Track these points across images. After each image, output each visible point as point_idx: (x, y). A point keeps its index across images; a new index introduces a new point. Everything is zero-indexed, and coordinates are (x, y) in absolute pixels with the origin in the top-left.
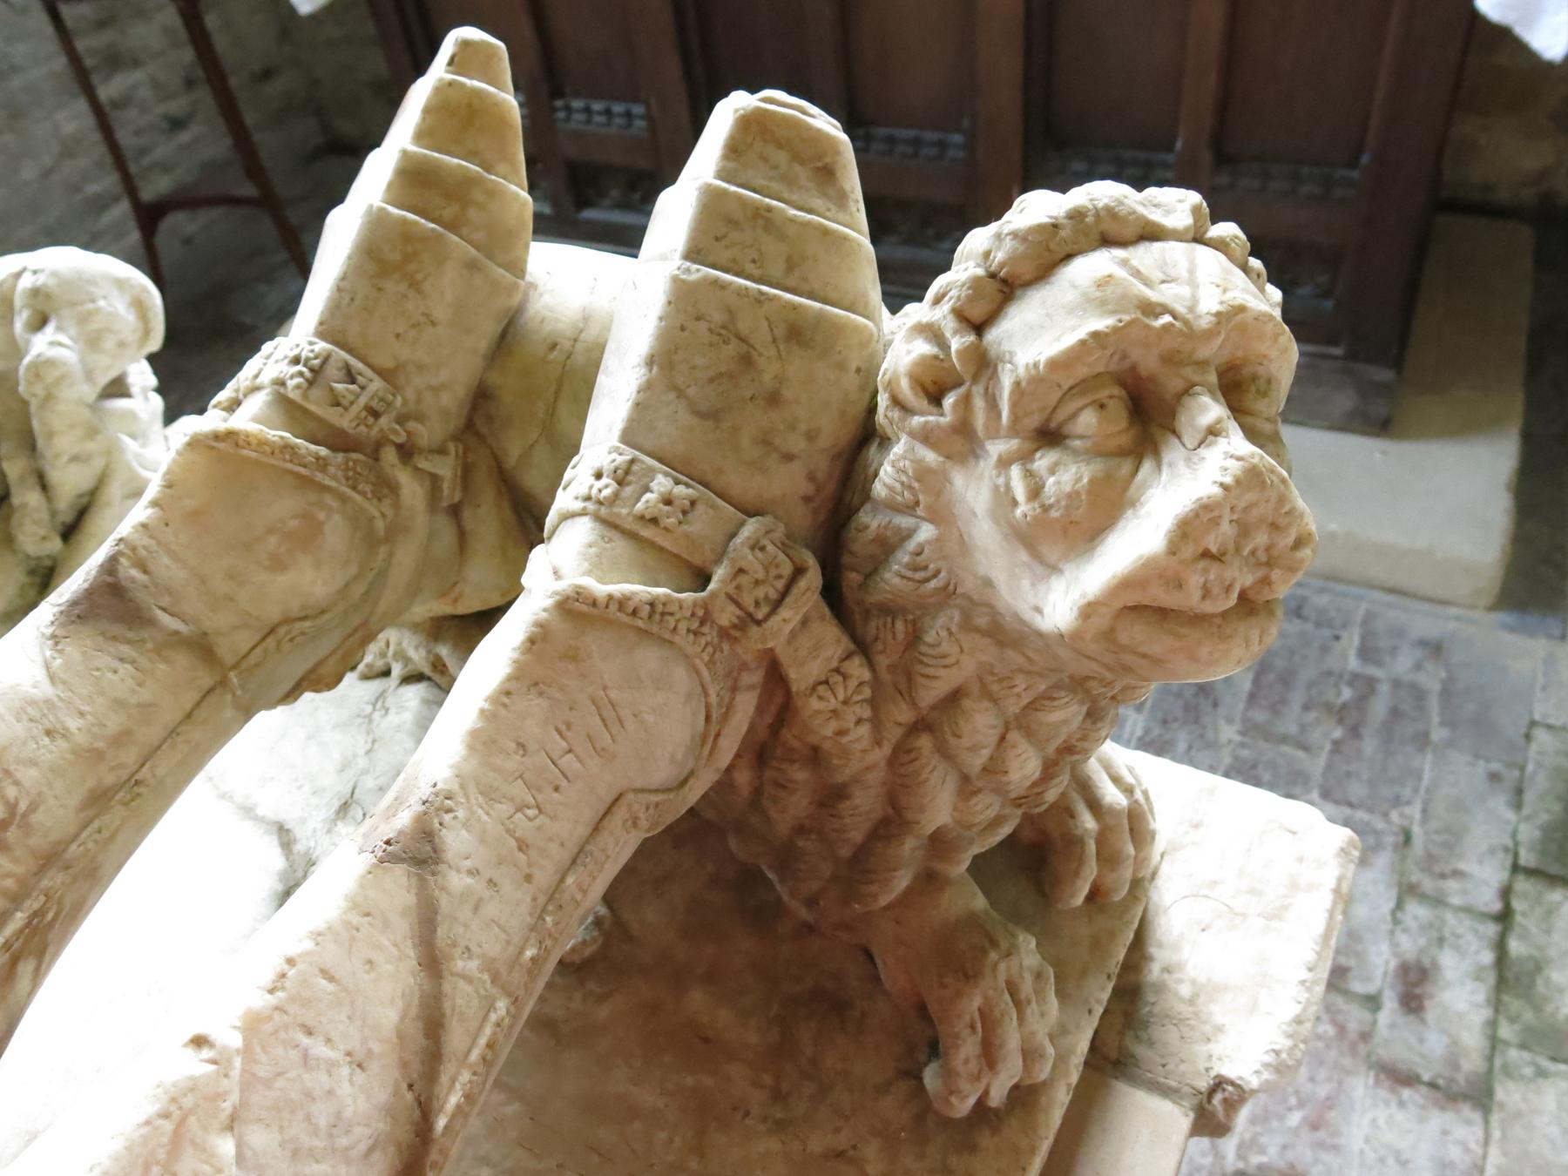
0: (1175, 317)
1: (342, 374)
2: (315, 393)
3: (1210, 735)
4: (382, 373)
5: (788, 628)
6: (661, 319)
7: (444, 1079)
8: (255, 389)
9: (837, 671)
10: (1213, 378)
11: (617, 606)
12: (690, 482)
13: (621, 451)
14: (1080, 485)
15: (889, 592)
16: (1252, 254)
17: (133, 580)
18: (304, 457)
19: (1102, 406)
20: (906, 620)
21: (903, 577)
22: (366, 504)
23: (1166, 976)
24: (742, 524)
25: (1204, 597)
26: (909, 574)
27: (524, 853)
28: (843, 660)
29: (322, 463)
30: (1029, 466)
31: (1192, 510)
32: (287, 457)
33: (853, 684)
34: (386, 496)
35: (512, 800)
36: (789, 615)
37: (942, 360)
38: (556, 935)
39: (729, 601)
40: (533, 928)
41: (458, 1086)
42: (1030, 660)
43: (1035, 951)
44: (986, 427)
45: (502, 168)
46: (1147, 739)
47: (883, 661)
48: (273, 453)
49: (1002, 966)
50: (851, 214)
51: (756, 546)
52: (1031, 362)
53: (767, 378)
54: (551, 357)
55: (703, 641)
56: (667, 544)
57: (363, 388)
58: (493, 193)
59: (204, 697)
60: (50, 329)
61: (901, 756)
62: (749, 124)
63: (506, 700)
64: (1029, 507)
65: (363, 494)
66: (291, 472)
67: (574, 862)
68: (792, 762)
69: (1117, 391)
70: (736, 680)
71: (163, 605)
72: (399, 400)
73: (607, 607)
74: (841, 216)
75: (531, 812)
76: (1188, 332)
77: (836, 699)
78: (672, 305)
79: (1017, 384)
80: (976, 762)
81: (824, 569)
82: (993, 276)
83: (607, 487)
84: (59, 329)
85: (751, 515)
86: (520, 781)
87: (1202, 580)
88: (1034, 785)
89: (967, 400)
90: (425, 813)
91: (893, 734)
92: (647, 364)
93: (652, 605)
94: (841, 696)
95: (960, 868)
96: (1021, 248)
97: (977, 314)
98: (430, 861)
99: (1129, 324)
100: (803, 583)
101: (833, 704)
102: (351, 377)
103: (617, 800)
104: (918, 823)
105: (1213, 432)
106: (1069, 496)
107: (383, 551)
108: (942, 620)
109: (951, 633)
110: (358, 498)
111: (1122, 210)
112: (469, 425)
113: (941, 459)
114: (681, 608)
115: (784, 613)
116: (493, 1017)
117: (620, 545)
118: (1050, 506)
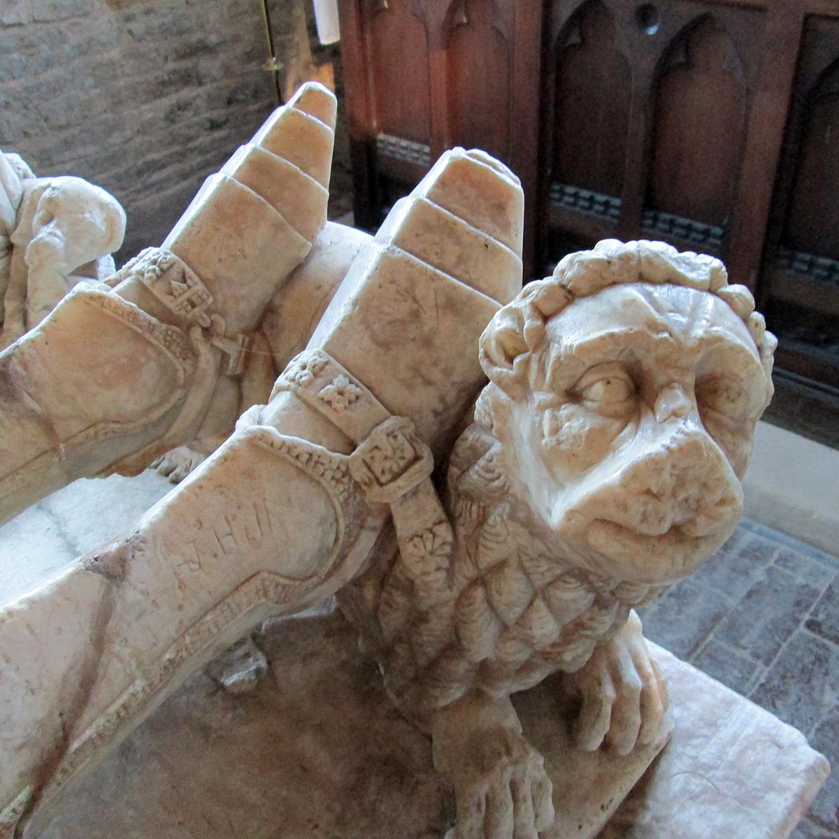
0: (671, 335)
1: (180, 277)
2: (160, 284)
3: (816, 695)
4: (203, 280)
5: (401, 493)
6: (369, 278)
7: (86, 717)
8: (129, 275)
9: (430, 530)
10: (690, 379)
11: (287, 449)
12: (360, 384)
13: (322, 355)
14: (582, 431)
15: (471, 484)
16: (756, 309)
17: (16, 373)
18: (141, 321)
19: (609, 382)
20: (479, 506)
21: (480, 476)
22: (175, 361)
23: (654, 823)
24: (386, 418)
25: (642, 521)
26: (483, 473)
27: (182, 590)
28: (435, 524)
29: (151, 328)
30: (555, 413)
31: (643, 460)
32: (131, 319)
33: (438, 541)
34: (189, 358)
35: (184, 554)
36: (404, 484)
37: (517, 334)
38: (192, 651)
39: (363, 465)
40: (175, 641)
41: (94, 726)
42: (549, 549)
43: (542, 767)
44: (536, 383)
45: (313, 170)
46: (768, 687)
47: (462, 531)
48: (122, 315)
49: (510, 769)
50: (510, 237)
51: (391, 435)
52: (569, 344)
53: (426, 328)
54: (316, 293)
55: (341, 488)
56: (334, 419)
57: (189, 287)
58: (305, 185)
59: (42, 454)
60: (52, 225)
61: (463, 599)
62: (458, 168)
63: (198, 491)
64: (550, 439)
65: (174, 353)
66: (130, 328)
67: (215, 606)
68: (397, 588)
69: (622, 375)
70: (363, 521)
71: (30, 391)
72: (211, 300)
73: (280, 449)
74: (503, 237)
75: (194, 566)
76: (679, 347)
77: (425, 547)
78: (378, 271)
79: (558, 358)
80: (512, 616)
81: (436, 457)
82: (563, 287)
83: (306, 375)
84: (58, 226)
85: (393, 413)
86: (192, 544)
87: (642, 509)
88: (554, 645)
89: (527, 363)
90: (125, 548)
91: (461, 582)
92: (353, 304)
93: (311, 455)
94: (429, 548)
95: (502, 691)
96: (584, 272)
97: (546, 309)
98: (118, 578)
99: (638, 333)
100: (417, 466)
101: (423, 552)
102: (184, 279)
103: (254, 575)
104: (469, 651)
105: (676, 414)
106: (575, 437)
107: (179, 393)
108: (499, 510)
109: (503, 520)
110: (170, 355)
111: (657, 262)
112: (259, 327)
113: (509, 399)
114: (330, 462)
115: (400, 482)
116: (131, 690)
117: (304, 412)
118: (563, 442)
